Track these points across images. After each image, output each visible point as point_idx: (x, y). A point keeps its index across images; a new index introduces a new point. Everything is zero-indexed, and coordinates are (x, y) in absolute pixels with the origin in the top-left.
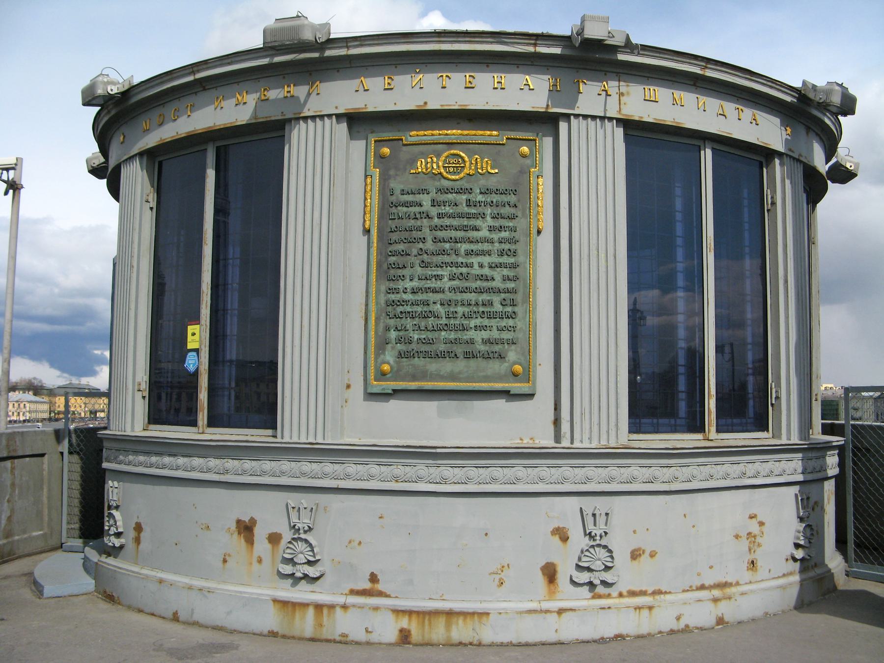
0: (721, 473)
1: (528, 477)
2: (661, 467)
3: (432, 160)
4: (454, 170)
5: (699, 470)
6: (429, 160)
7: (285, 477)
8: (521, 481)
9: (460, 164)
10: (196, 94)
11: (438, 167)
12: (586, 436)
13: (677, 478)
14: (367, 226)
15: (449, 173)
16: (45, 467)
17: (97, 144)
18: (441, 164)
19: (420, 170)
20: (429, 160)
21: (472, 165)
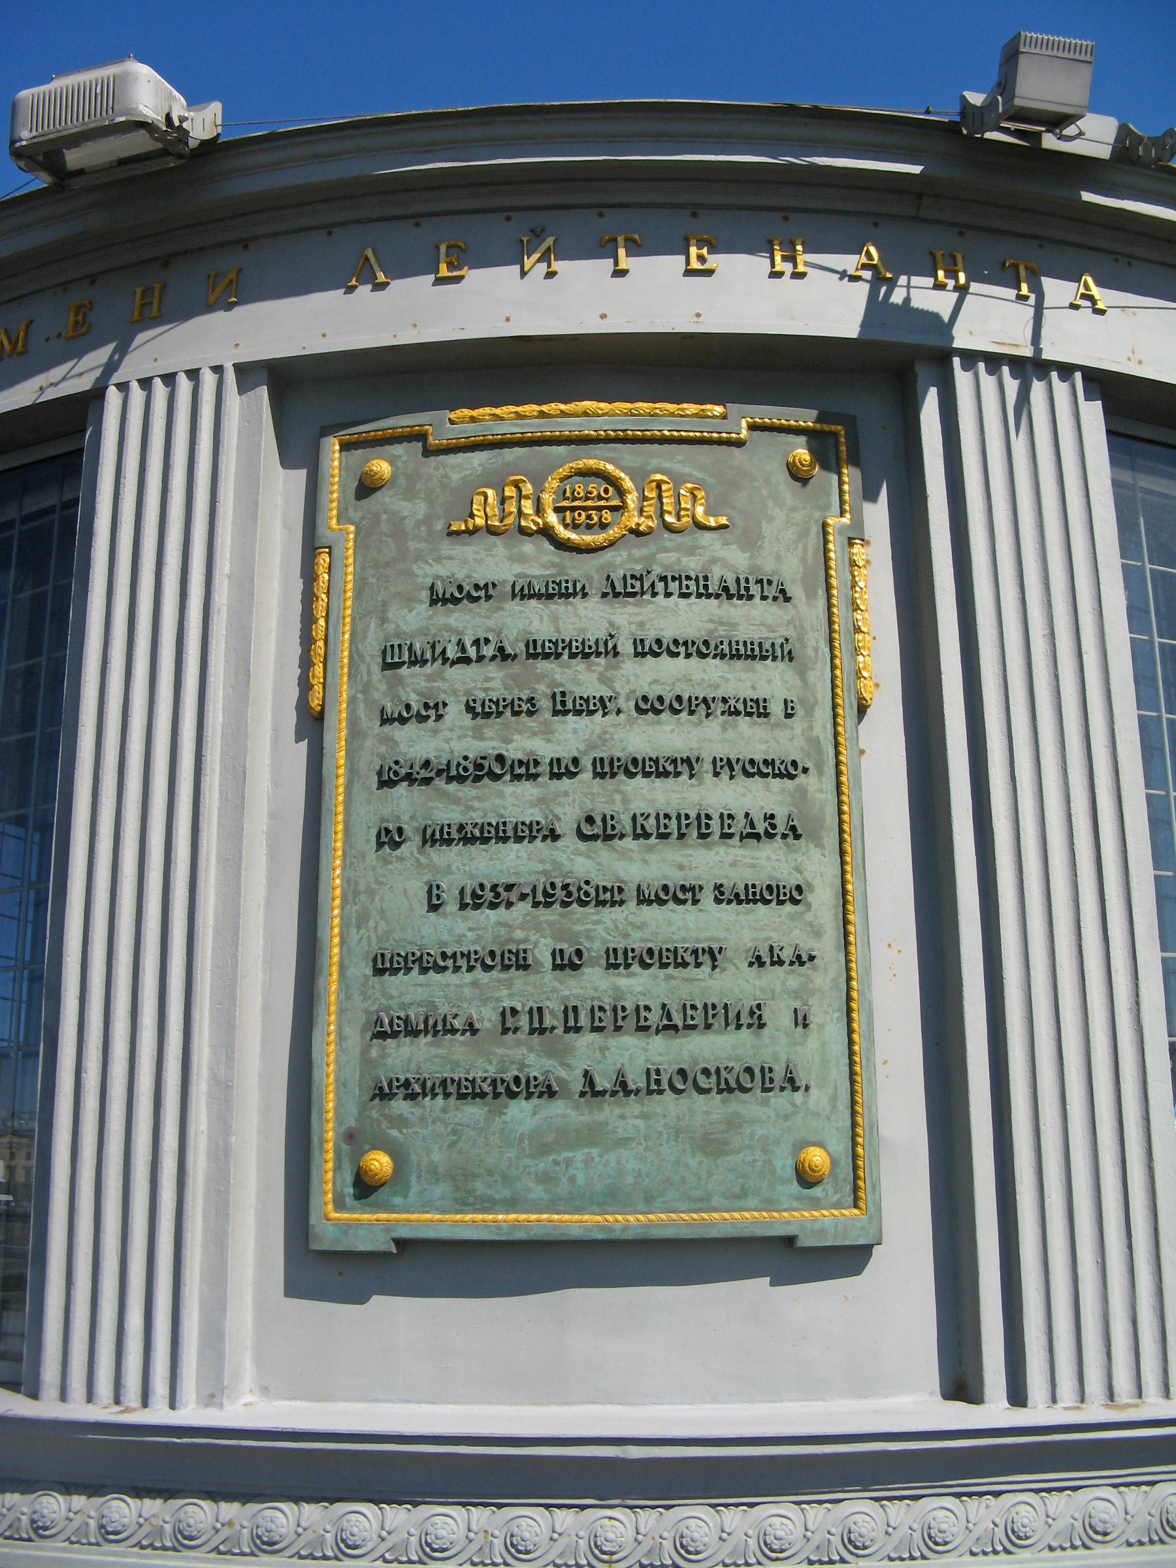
0: (1142, 1519)
1: (383, 1539)
2: (1037, 1491)
3: (520, 490)
4: (589, 517)
5: (1120, 1506)
6: (510, 491)
7: (1109, 1549)
8: (277, 1547)
9: (607, 499)
10: (65, 290)
11: (539, 510)
12: (160, 1387)
13: (1105, 1534)
14: (315, 703)
15: (575, 527)
16: (723, 1535)
17: (922, 417)
18: (547, 498)
19: (480, 521)
20: (510, 491)
21: (645, 503)
